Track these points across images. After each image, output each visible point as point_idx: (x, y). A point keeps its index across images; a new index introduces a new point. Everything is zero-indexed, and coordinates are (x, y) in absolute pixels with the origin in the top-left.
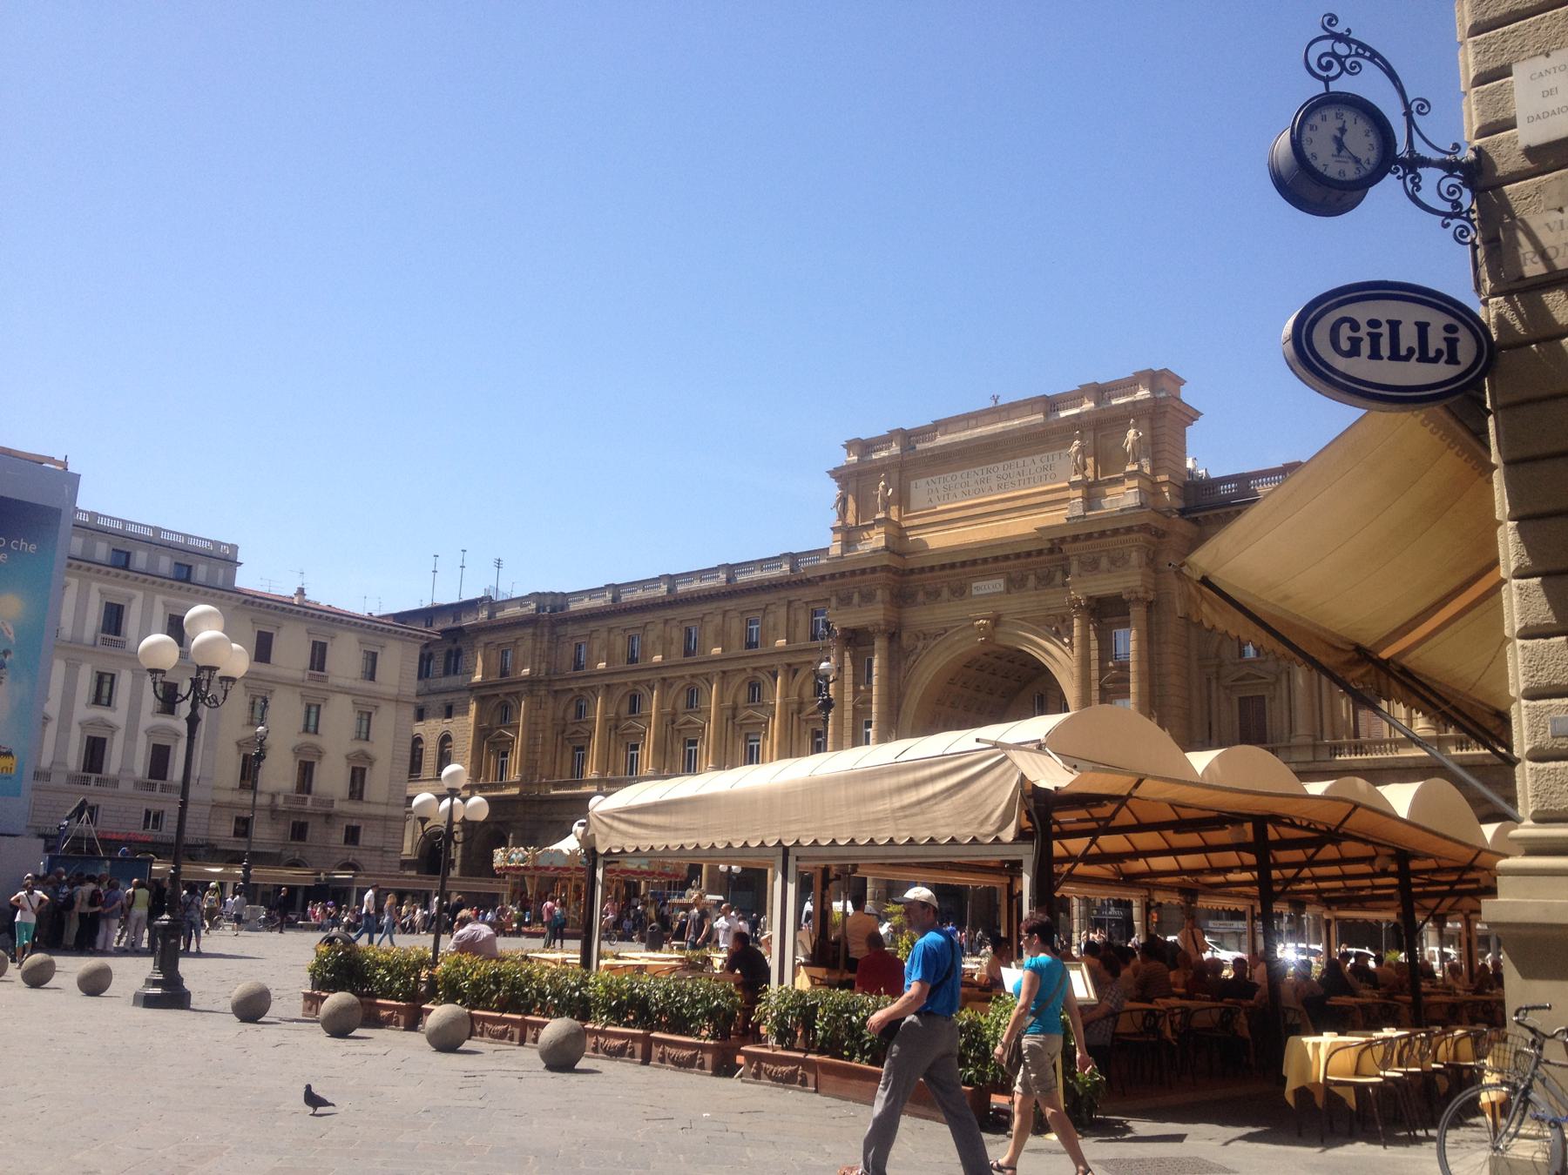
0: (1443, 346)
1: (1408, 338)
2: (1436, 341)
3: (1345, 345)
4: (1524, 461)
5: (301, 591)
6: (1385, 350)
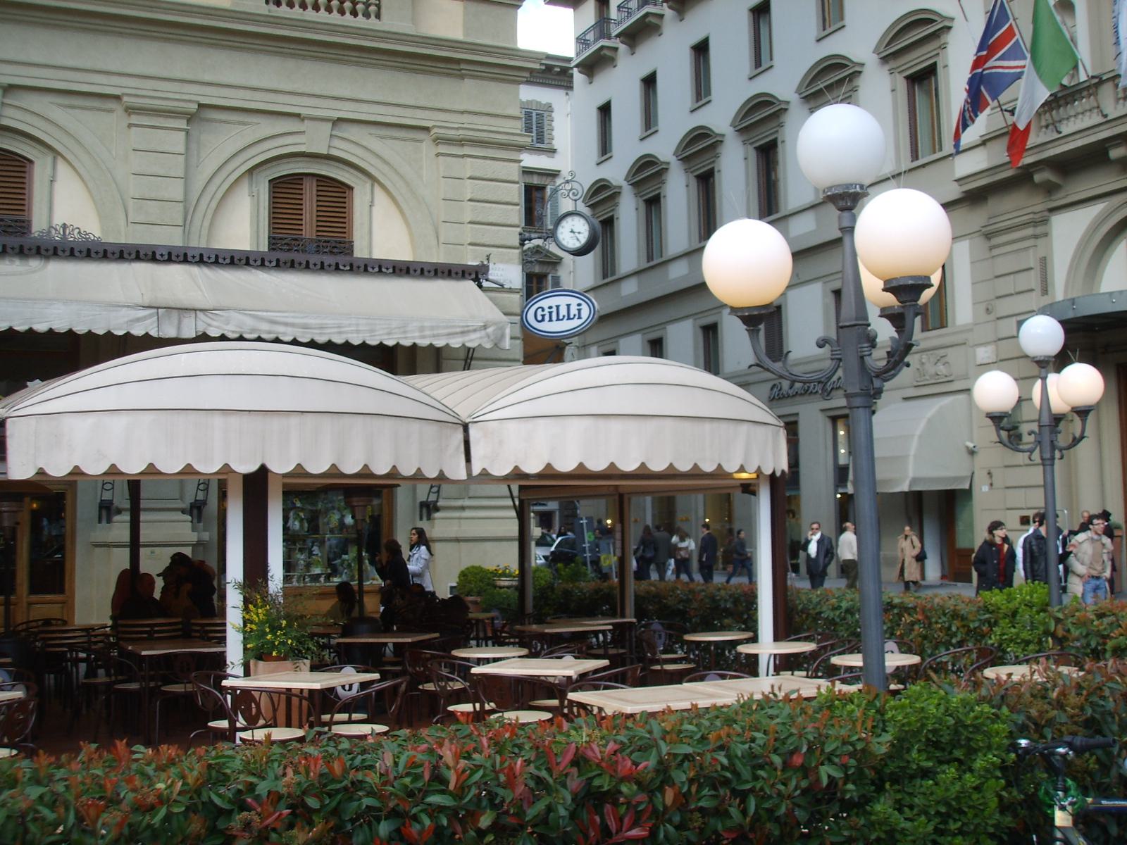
0: (577, 313)
1: (563, 312)
2: (574, 311)
3: (540, 318)
4: (1022, 379)
5: (908, 365)
6: (554, 317)
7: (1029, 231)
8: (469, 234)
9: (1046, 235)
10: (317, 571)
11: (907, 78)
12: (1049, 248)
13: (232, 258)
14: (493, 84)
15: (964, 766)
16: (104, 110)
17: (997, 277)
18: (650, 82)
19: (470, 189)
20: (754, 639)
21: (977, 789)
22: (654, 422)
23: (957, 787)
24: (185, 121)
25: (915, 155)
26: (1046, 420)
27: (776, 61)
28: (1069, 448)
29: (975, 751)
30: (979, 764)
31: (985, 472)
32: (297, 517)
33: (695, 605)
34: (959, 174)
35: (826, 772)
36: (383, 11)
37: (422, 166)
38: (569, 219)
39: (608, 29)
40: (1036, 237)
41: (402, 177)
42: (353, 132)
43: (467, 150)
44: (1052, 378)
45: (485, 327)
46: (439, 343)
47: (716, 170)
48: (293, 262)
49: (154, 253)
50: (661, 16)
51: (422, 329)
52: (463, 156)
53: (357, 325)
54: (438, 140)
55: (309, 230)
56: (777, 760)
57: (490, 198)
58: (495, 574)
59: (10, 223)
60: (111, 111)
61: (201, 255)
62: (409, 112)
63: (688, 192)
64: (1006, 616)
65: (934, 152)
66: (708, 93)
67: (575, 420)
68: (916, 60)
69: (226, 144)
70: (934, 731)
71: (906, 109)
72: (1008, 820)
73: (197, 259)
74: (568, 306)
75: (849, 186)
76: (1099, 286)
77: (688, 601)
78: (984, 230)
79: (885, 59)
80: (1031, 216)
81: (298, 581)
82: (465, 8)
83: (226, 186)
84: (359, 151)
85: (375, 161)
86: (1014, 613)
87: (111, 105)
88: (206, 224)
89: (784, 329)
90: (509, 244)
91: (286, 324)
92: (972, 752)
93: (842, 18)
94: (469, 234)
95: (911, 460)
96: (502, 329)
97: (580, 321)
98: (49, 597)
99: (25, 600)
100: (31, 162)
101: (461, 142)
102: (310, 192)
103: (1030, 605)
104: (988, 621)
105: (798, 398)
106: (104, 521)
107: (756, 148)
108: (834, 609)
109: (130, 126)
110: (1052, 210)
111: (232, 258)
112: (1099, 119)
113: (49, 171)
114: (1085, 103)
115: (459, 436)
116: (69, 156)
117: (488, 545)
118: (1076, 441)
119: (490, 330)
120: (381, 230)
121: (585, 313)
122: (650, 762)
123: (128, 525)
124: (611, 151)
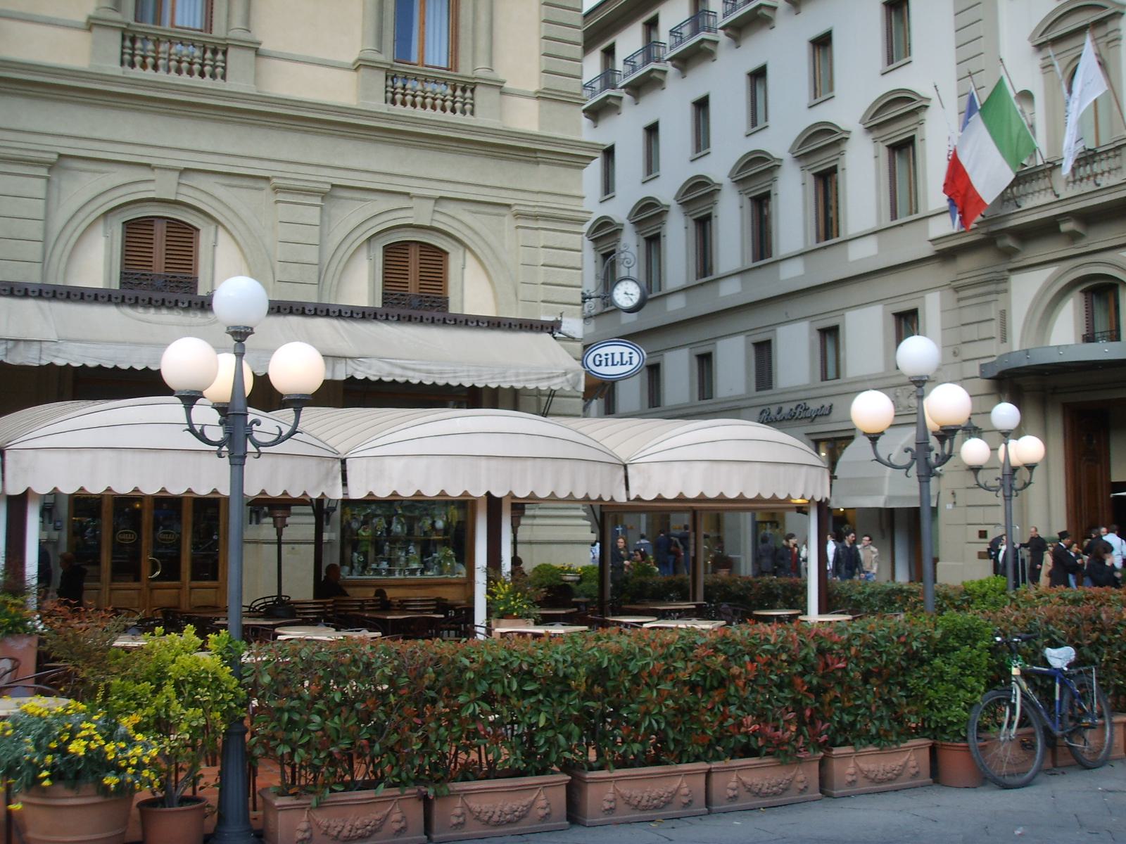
1: (617, 358)
2: (626, 358)
3: (598, 363)
7: (992, 287)
8: (543, 292)
9: (1006, 291)
10: (415, 566)
11: (889, 147)
12: (1008, 302)
13: (364, 313)
14: (562, 169)
15: (973, 647)
16: (256, 189)
17: (964, 343)
18: (652, 130)
19: (543, 256)
20: (805, 613)
21: (979, 656)
22: (747, 466)
23: (969, 655)
24: (320, 199)
25: (894, 216)
26: (1007, 471)
27: (771, 122)
28: (1021, 489)
29: (977, 640)
30: (980, 644)
31: (949, 493)
32: (399, 522)
33: (754, 591)
34: (933, 235)
35: (915, 645)
36: (477, 109)
37: (503, 235)
38: (624, 283)
39: (614, 79)
40: (997, 292)
41: (489, 245)
42: (451, 208)
43: (541, 224)
44: (1012, 443)
45: (565, 374)
46: (518, 386)
47: (713, 215)
48: (410, 317)
49: (304, 308)
50: (664, 72)
51: (517, 375)
52: (537, 229)
53: (468, 371)
54: (518, 216)
55: (413, 288)
56: (895, 638)
57: (558, 263)
58: (562, 570)
59: (181, 280)
60: (261, 189)
61: (340, 311)
62: (495, 192)
63: (687, 233)
64: (979, 597)
65: (911, 214)
66: (708, 145)
67: (698, 463)
68: (898, 133)
69: (353, 216)
70: (960, 630)
71: (887, 169)
72: (991, 673)
73: (337, 314)
74: (622, 354)
75: (922, 377)
76: (1049, 339)
77: (749, 589)
78: (954, 284)
79: (870, 129)
80: (994, 275)
81: (400, 574)
82: (540, 106)
83: (350, 251)
84: (456, 224)
85: (467, 232)
86: (984, 595)
87: (262, 184)
88: (335, 282)
89: (773, 360)
90: (574, 302)
91: (414, 370)
92: (976, 640)
93: (831, 89)
94: (543, 292)
95: (887, 480)
96: (578, 375)
97: (632, 367)
98: (206, 583)
99: (187, 586)
100: (198, 230)
101: (536, 217)
102: (414, 255)
103: (994, 590)
104: (967, 600)
105: (784, 423)
106: (254, 522)
107: (751, 198)
108: (860, 593)
109: (277, 202)
110: (1011, 270)
111: (364, 313)
112: (1052, 199)
113: (212, 237)
114: (1042, 184)
115: (622, 473)
116: (229, 227)
117: (554, 546)
118: (1026, 485)
119: (569, 376)
120: (471, 291)
121: (636, 360)
122: (845, 636)
123: (313, 527)
124: (613, 191)
